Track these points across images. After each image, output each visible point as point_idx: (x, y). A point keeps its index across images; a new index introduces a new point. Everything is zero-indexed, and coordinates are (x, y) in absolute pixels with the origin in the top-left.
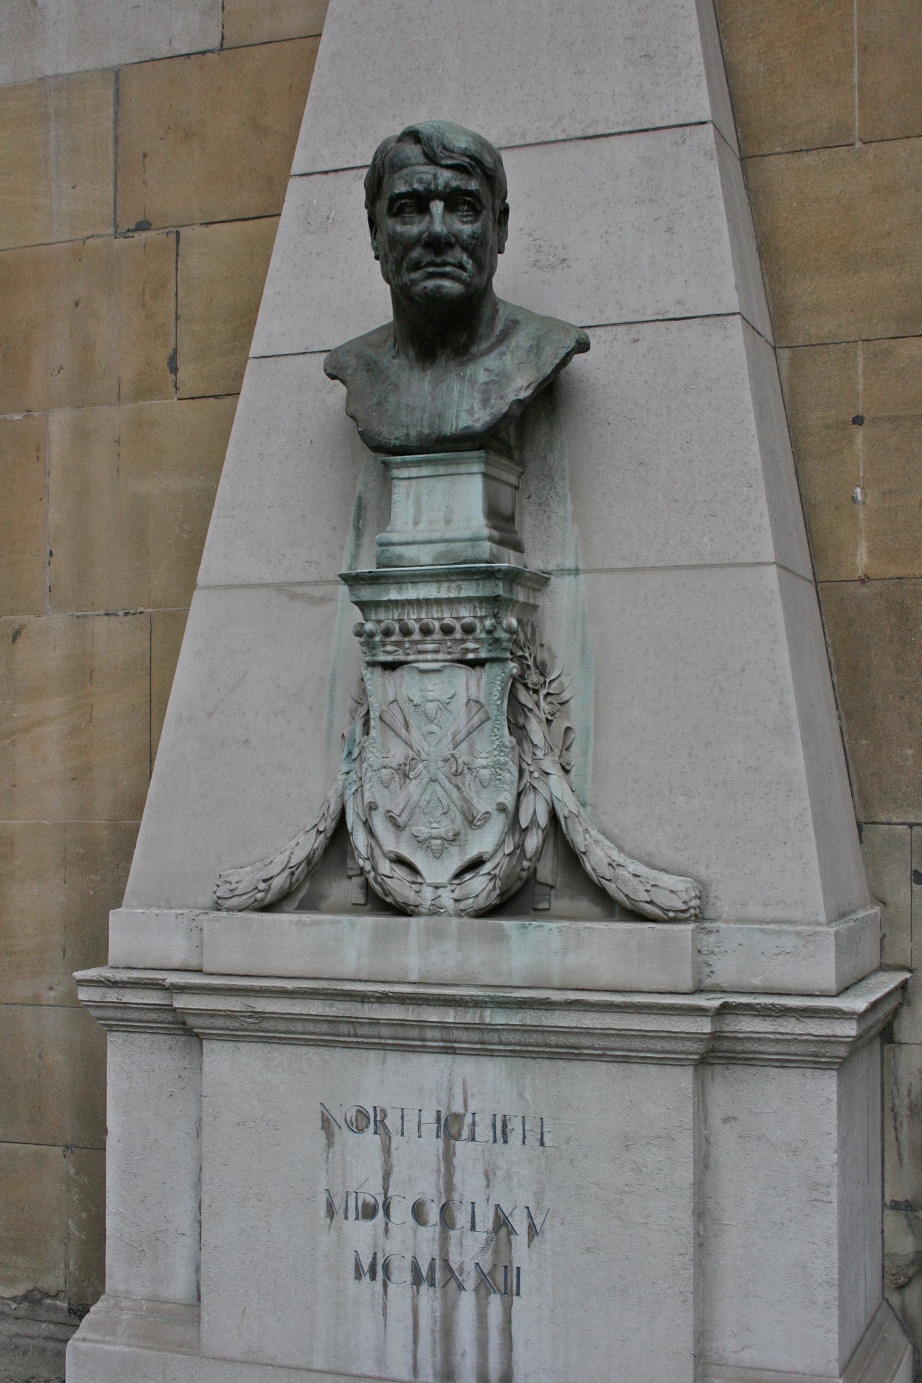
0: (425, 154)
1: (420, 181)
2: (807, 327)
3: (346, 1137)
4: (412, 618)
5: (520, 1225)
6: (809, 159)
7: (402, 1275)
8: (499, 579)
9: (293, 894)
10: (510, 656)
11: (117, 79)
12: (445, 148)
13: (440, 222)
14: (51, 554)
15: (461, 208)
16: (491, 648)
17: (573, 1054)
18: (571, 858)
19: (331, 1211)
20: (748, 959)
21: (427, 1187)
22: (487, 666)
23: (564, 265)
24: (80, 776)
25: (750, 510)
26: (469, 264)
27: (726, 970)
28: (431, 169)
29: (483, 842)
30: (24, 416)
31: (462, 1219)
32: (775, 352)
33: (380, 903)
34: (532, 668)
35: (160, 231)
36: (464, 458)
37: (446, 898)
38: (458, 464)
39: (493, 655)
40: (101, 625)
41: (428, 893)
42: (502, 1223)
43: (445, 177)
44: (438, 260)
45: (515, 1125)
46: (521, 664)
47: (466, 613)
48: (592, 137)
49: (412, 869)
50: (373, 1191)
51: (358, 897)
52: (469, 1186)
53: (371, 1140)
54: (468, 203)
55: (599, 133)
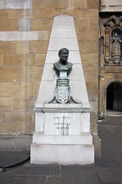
3: (56, 119)
4: (62, 82)
5: (69, 124)
6: (83, 54)
7: (60, 128)
9: (51, 102)
13: (64, 55)
17: (73, 112)
18: (72, 99)
19: (55, 124)
20: (85, 106)
21: (62, 122)
24: (26, 94)
27: (83, 107)
29: (66, 98)
31: (65, 124)
33: (58, 103)
37: (64, 102)
40: (28, 83)
41: (62, 102)
42: (68, 124)
45: (69, 117)
47: (66, 82)
49: (61, 100)
50: (58, 122)
51: (56, 102)
52: (65, 122)
53: (58, 119)
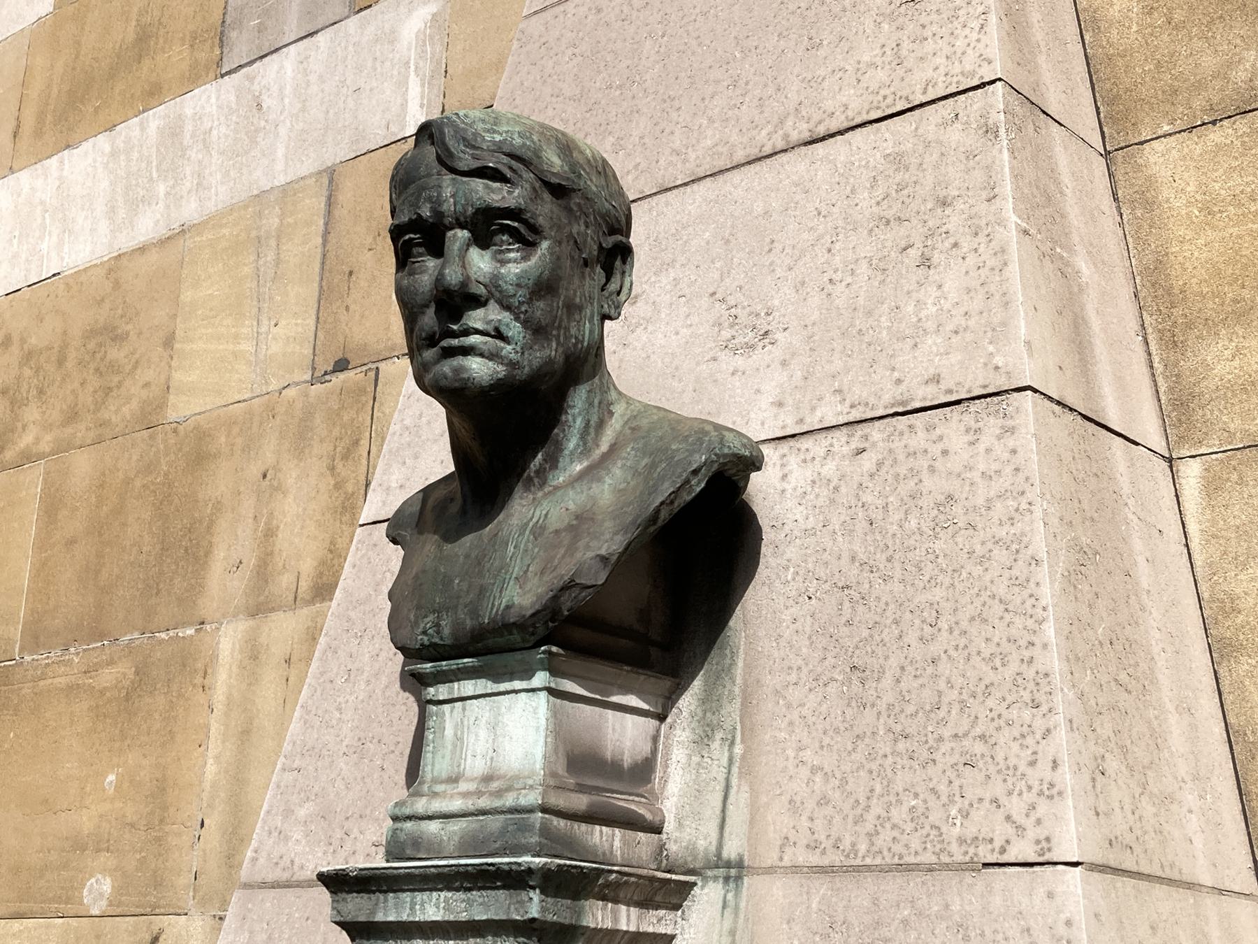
2: (1225, 418)
8: (533, 888)
11: (331, 181)
14: (202, 825)
15: (497, 239)
25: (1035, 753)
26: (515, 329)
32: (1171, 467)
35: (359, 370)
48: (823, 139)
55: (833, 129)
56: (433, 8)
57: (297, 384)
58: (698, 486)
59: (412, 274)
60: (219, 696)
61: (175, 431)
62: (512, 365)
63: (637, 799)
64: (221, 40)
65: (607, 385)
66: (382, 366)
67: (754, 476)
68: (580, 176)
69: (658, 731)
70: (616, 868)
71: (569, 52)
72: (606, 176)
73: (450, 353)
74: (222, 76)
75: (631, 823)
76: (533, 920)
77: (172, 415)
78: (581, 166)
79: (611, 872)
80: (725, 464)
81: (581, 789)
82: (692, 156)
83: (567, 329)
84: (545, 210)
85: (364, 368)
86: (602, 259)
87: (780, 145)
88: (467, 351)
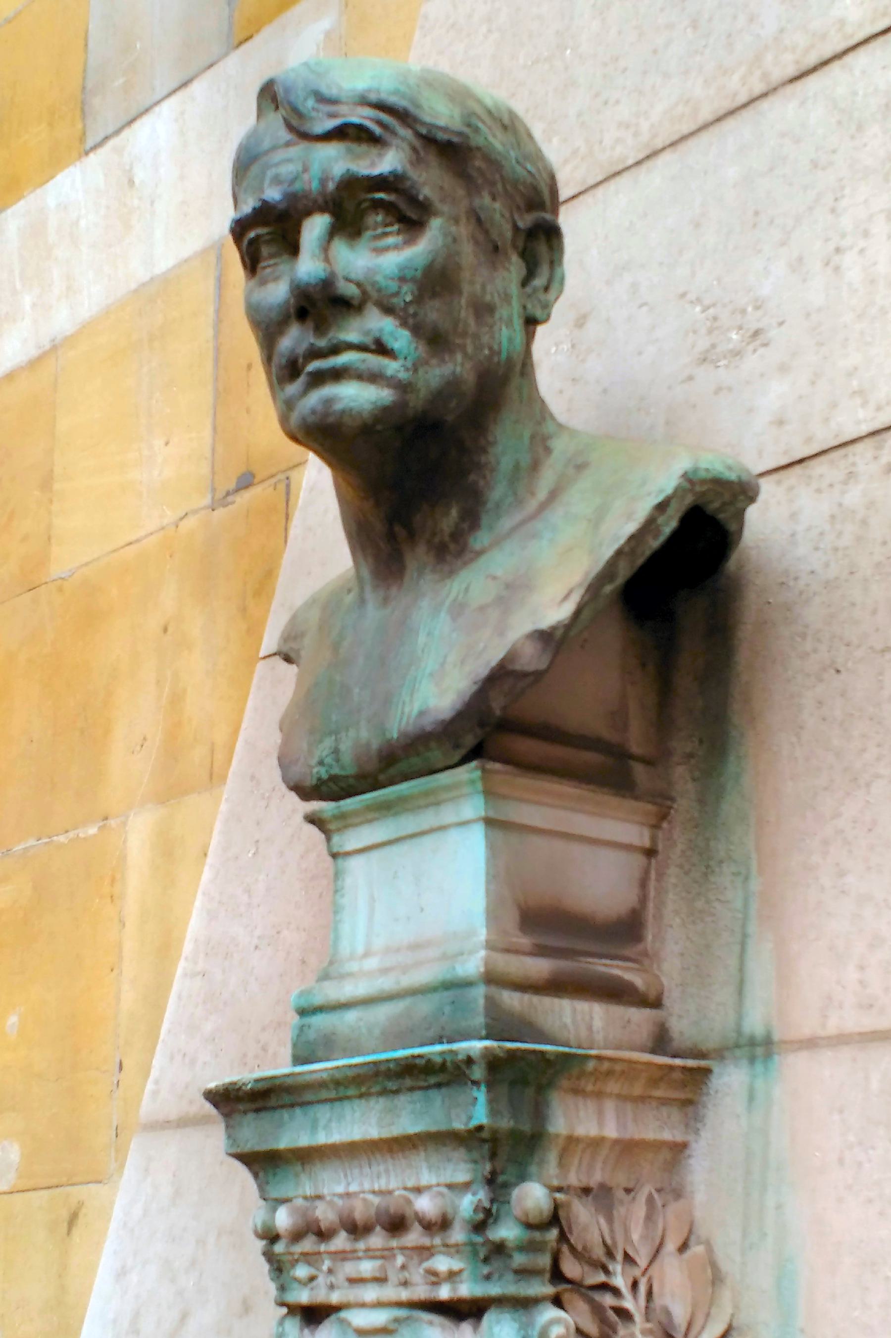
0: (290, 127)
1: (277, 180)
8: (476, 1083)
10: (549, 1290)
12: (322, 99)
16: (486, 1270)
22: (489, 1318)
23: (758, 342)
26: (400, 339)
28: (299, 149)
30: (100, 828)
34: (638, 1317)
36: (448, 788)
38: (438, 804)
39: (494, 1290)
43: (334, 162)
44: (322, 343)
46: (597, 1310)
54: (378, 205)
55: (828, 53)
56: (326, 23)
57: (195, 512)
58: (669, 525)
59: (263, 283)
60: (131, 907)
61: (60, 590)
62: (403, 387)
63: (620, 963)
64: (83, 111)
65: (542, 412)
66: (290, 473)
67: (752, 513)
68: (477, 130)
69: (646, 872)
70: (593, 1052)
71: (484, 29)
72: (515, 132)
73: (319, 379)
74: (87, 153)
75: (615, 992)
76: (480, 1128)
77: (56, 570)
78: (479, 118)
79: (587, 1057)
80: (703, 494)
81: (541, 951)
82: (645, 126)
83: (476, 337)
84: (430, 181)
85: (273, 481)
86: (520, 243)
87: (759, 88)
88: (338, 375)
